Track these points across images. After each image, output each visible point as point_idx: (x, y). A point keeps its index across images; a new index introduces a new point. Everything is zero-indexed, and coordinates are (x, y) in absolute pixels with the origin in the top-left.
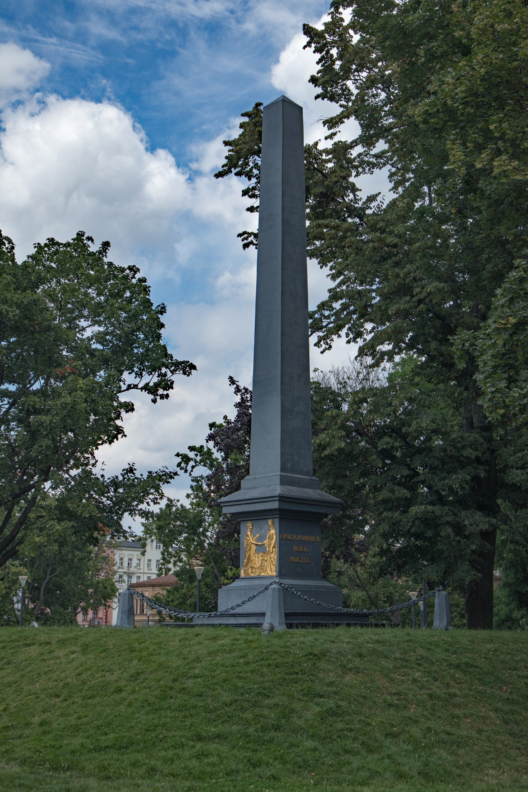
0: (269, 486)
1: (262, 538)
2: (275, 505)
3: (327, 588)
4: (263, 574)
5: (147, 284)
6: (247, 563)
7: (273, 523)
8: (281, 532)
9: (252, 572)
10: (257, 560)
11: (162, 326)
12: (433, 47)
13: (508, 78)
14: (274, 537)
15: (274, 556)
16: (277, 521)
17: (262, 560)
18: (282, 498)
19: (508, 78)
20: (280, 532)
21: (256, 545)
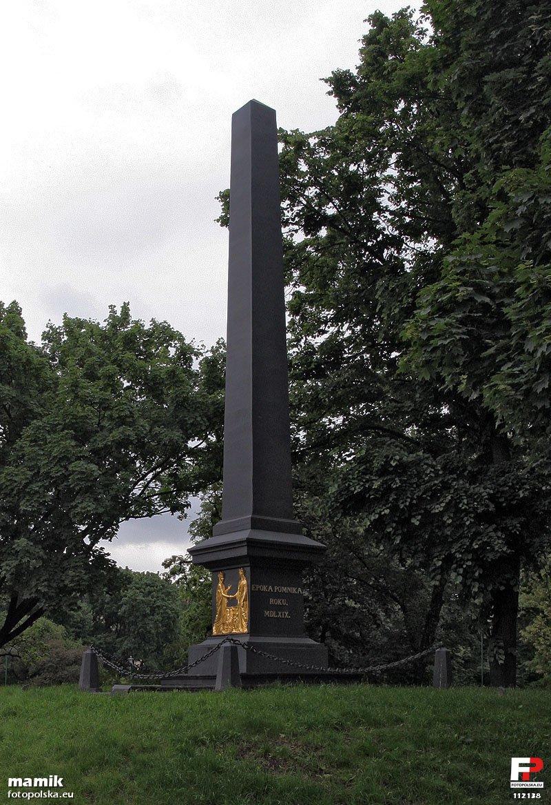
0: (164, 678)
1: (233, 591)
2: (244, 551)
3: (309, 646)
4: (234, 631)
5: (59, 323)
6: (219, 619)
7: (245, 573)
8: (253, 581)
9: (224, 629)
10: (229, 614)
11: (340, 83)
12: (449, 480)
13: (199, 717)
14: (245, 589)
15: (245, 613)
16: (248, 569)
17: (234, 615)
18: (250, 543)
19: (199, 717)
20: (251, 583)
21: (228, 598)
